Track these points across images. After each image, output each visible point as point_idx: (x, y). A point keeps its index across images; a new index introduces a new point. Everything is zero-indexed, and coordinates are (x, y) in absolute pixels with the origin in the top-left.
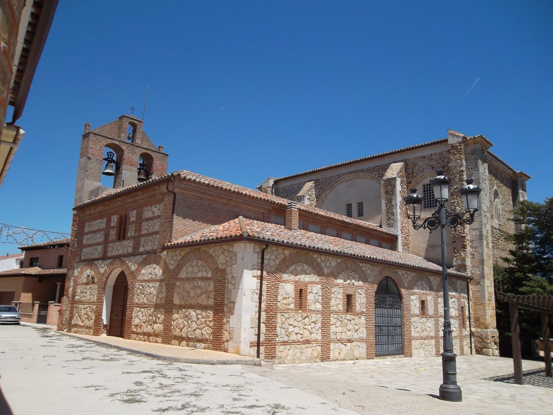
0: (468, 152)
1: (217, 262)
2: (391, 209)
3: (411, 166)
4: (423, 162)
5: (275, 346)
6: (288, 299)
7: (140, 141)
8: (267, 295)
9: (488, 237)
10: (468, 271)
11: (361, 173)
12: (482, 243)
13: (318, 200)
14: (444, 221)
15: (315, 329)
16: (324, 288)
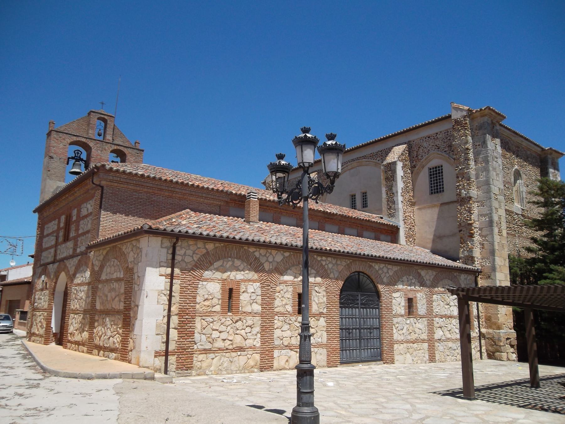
0: (475, 126)
1: (127, 260)
2: (391, 197)
3: (415, 148)
5: (193, 355)
6: (211, 300)
7: (111, 137)
8: (180, 296)
10: (476, 263)
11: (363, 160)
12: (492, 230)
14: (306, 192)
15: (251, 334)
16: (264, 287)
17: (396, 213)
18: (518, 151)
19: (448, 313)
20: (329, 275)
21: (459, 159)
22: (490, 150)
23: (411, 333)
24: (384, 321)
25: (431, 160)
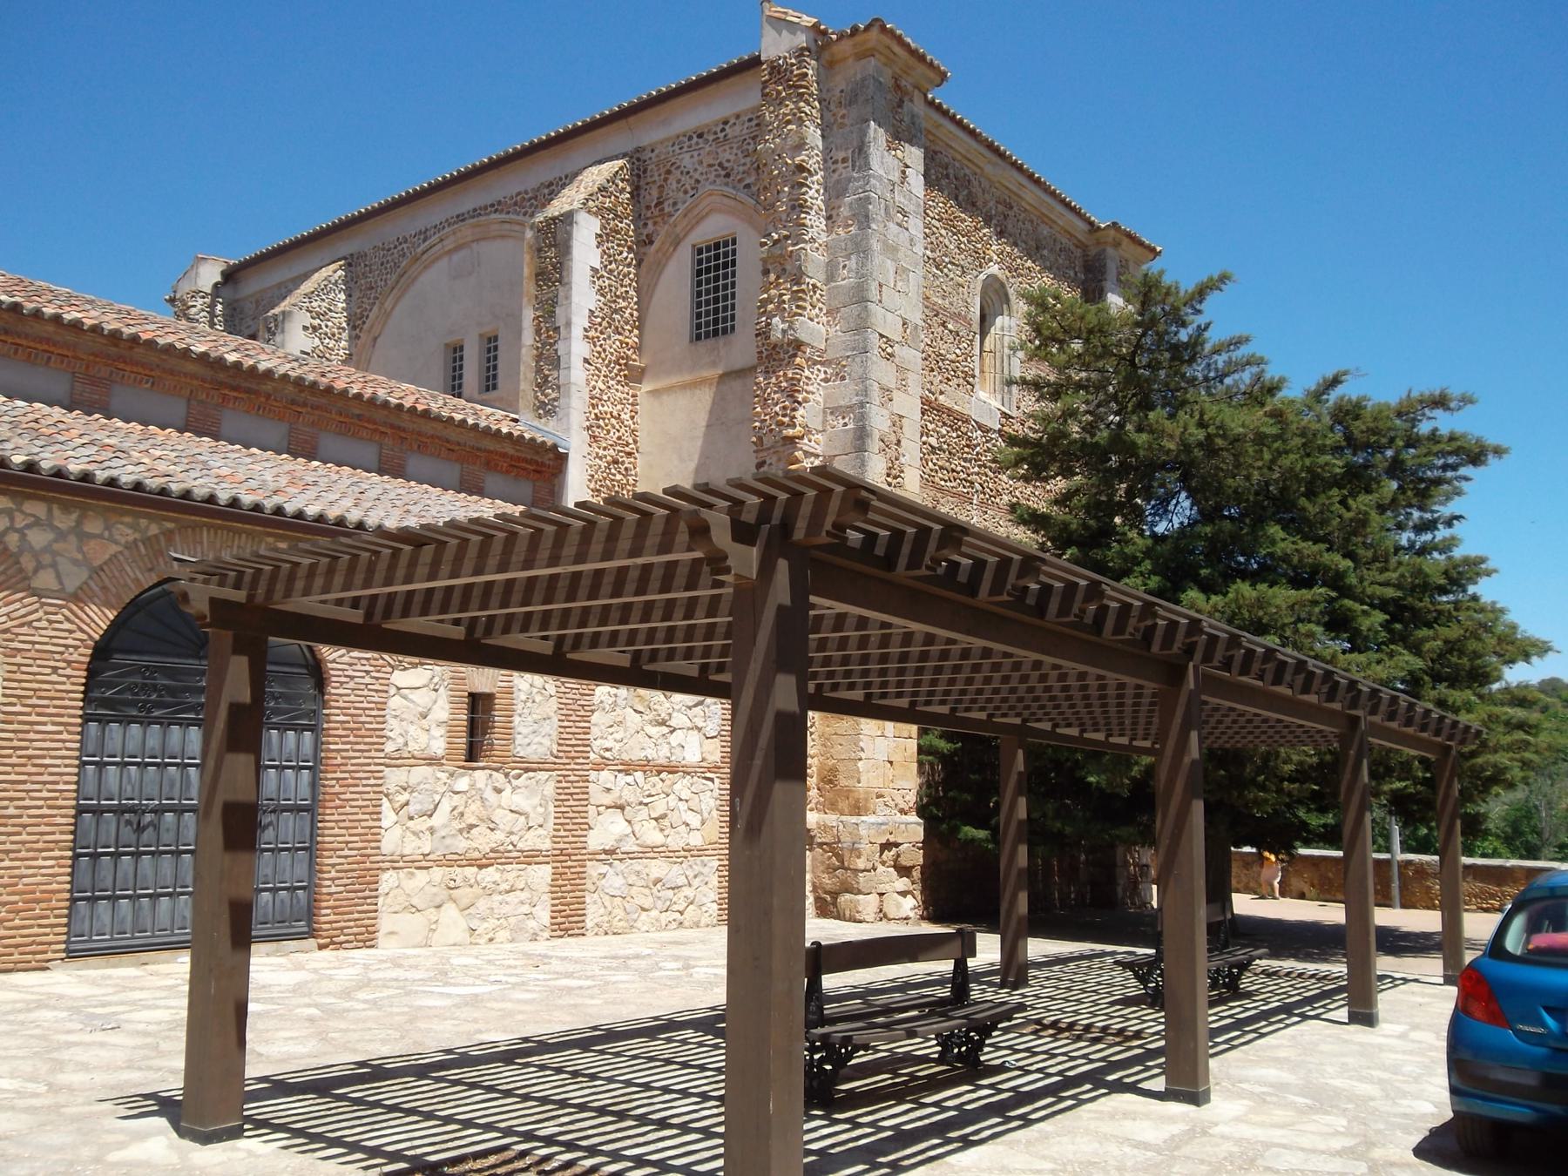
3: (656, 174)
4: (695, 153)
9: (898, 443)
11: (493, 216)
13: (358, 337)
17: (561, 400)
18: (1006, 217)
19: (660, 754)
20: (26, 578)
21: (773, 205)
22: (880, 178)
23: (471, 827)
24: (331, 782)
25: (703, 218)
